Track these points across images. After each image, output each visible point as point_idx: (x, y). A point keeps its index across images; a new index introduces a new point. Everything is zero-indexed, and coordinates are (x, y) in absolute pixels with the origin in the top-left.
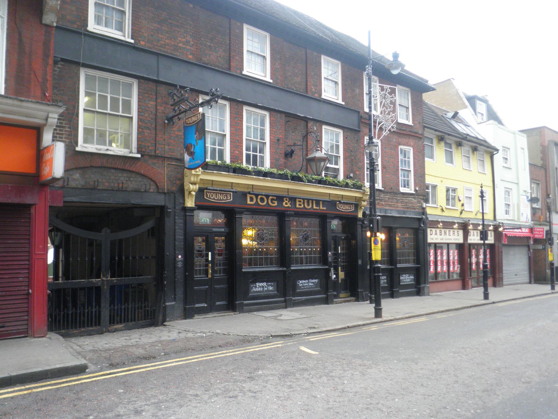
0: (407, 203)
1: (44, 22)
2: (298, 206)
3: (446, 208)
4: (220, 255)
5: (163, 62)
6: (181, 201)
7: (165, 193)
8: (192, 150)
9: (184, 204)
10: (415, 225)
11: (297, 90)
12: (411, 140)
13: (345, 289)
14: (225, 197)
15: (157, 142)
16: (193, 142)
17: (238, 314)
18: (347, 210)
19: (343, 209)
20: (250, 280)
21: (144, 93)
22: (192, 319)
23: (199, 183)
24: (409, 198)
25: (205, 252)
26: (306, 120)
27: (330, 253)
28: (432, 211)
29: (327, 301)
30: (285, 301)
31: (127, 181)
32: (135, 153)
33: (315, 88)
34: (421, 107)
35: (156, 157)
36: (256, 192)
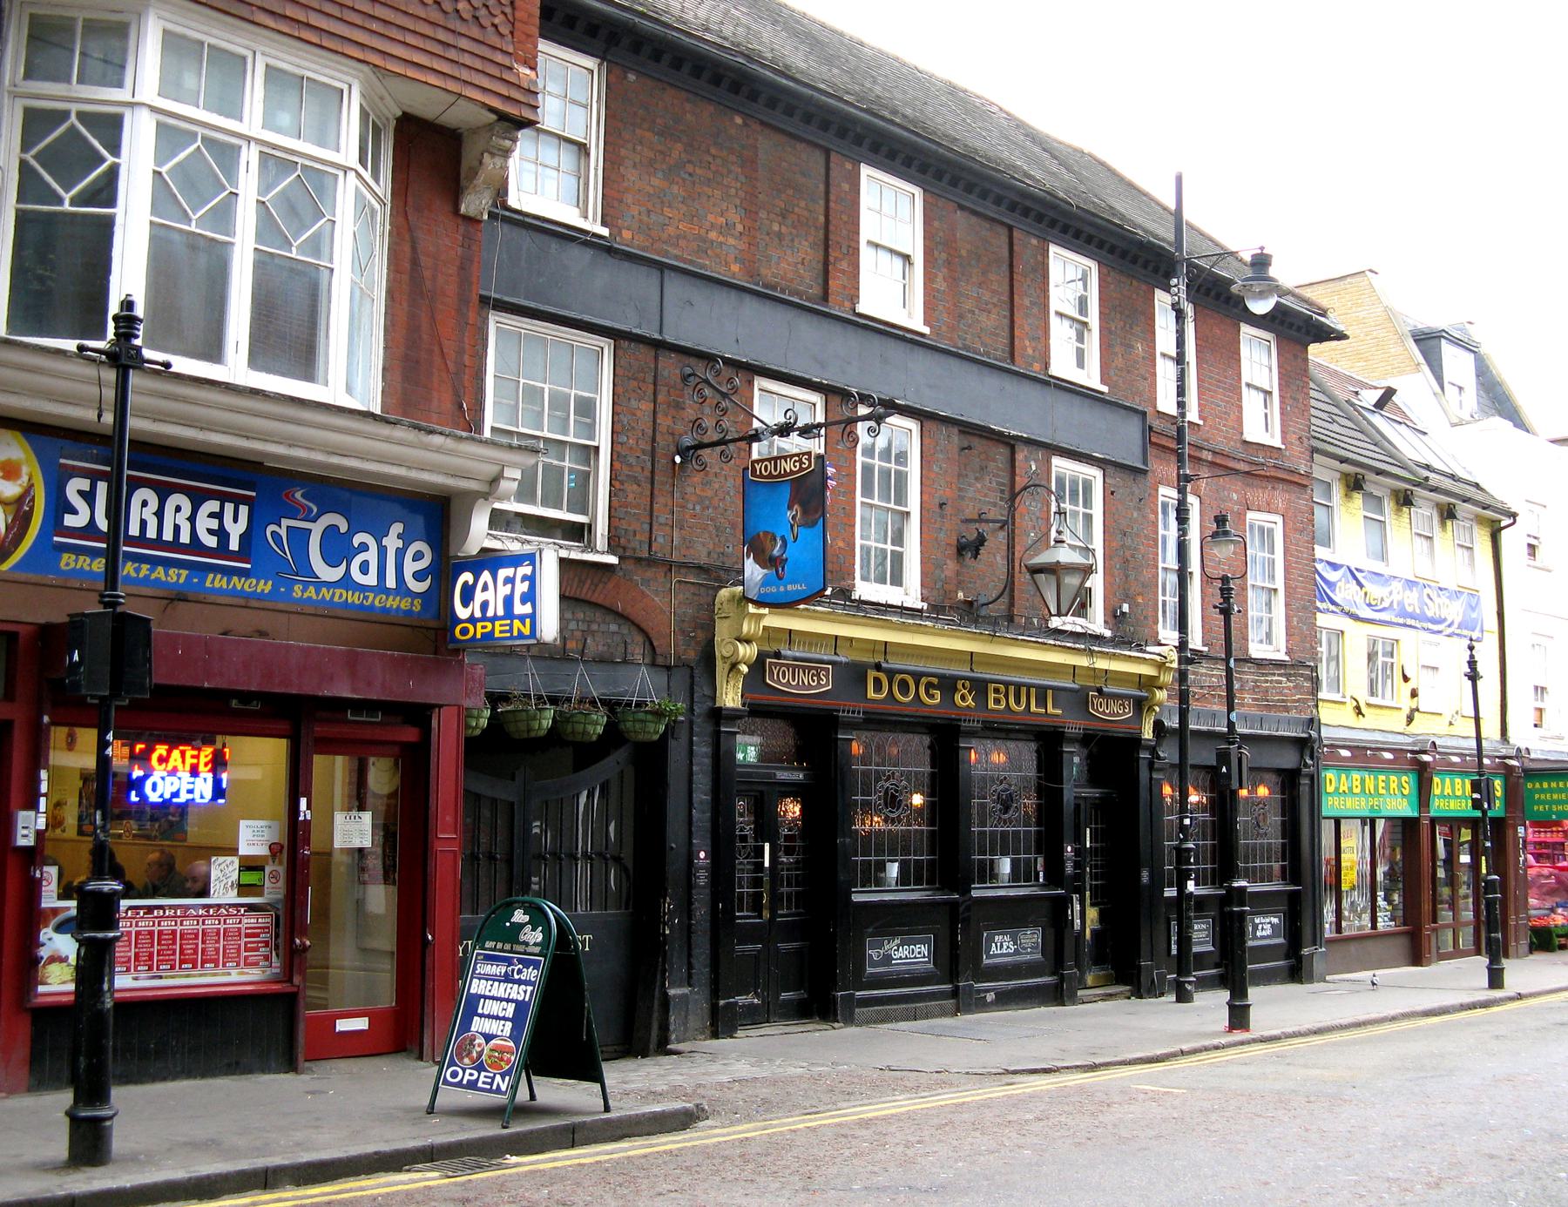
0: (1267, 691)
1: (463, 209)
2: (991, 705)
3: (1369, 705)
4: (789, 851)
5: (676, 289)
6: (707, 692)
7: (668, 668)
8: (776, 552)
9: (714, 698)
10: (1288, 760)
11: (987, 354)
12: (1277, 493)
13: (1098, 960)
14: (815, 678)
15: (654, 518)
16: (782, 530)
17: (841, 1028)
18: (1114, 715)
19: (1104, 713)
20: (867, 928)
21: (629, 379)
22: (732, 1037)
23: (760, 640)
24: (1274, 674)
25: (751, 842)
26: (1010, 443)
27: (1069, 849)
28: (1335, 720)
29: (1059, 995)
30: (955, 994)
31: (583, 631)
32: (603, 553)
33: (1034, 344)
34: (1305, 390)
35: (651, 562)
36: (895, 663)
